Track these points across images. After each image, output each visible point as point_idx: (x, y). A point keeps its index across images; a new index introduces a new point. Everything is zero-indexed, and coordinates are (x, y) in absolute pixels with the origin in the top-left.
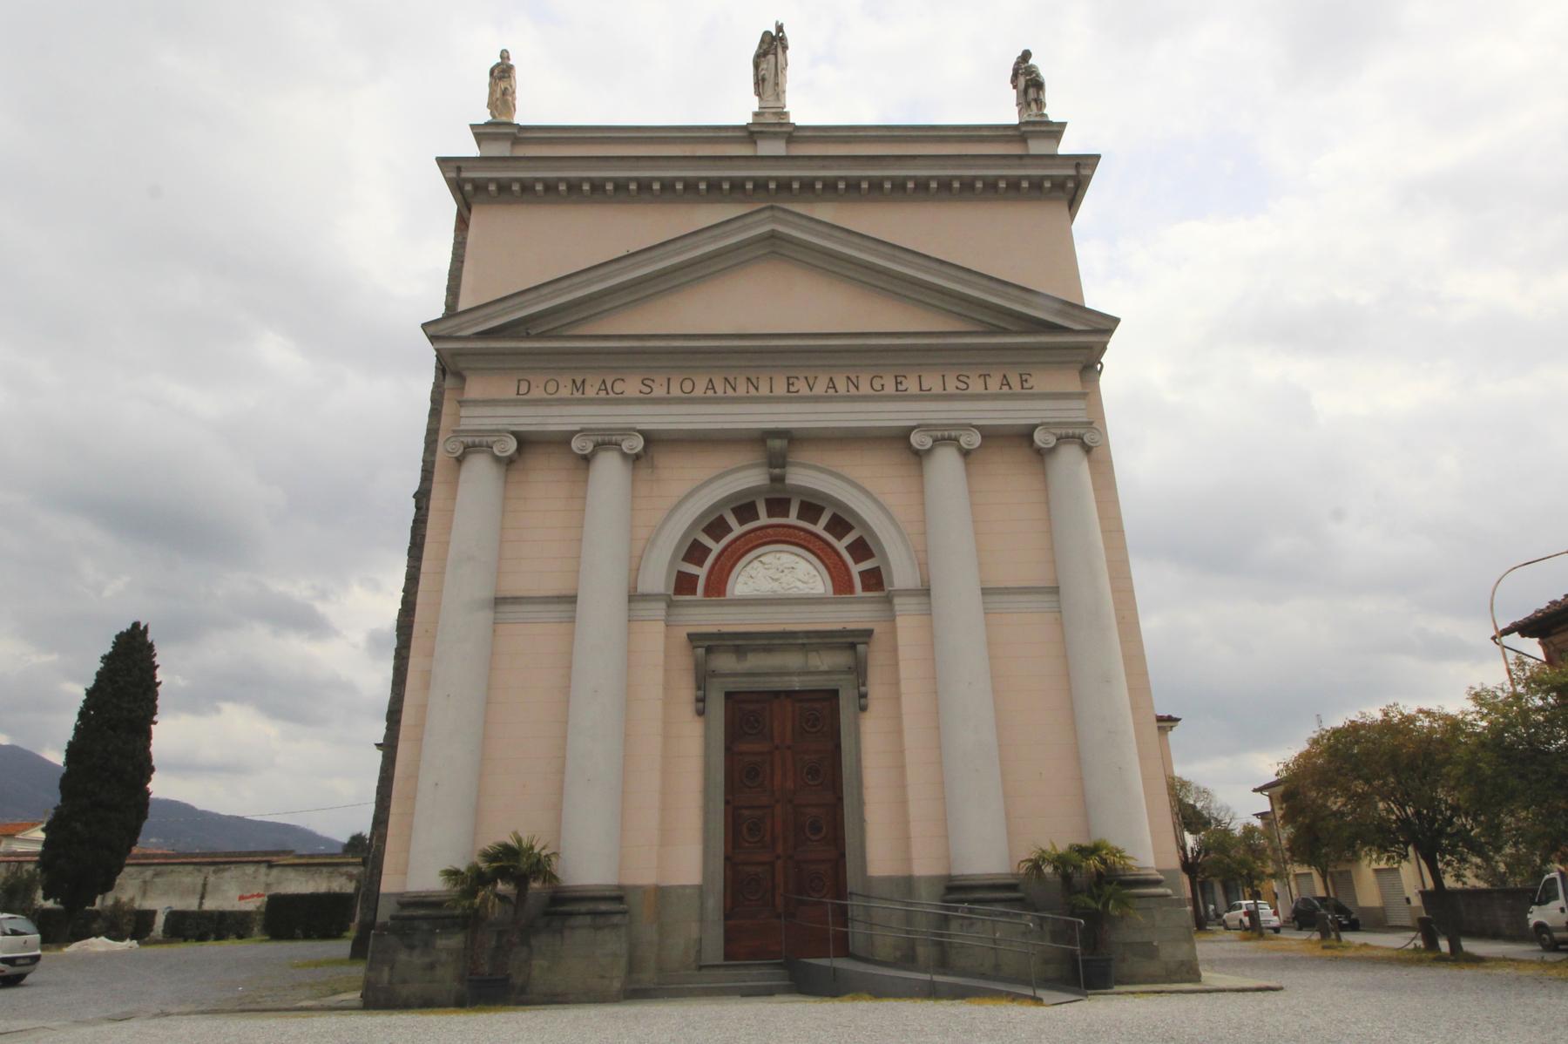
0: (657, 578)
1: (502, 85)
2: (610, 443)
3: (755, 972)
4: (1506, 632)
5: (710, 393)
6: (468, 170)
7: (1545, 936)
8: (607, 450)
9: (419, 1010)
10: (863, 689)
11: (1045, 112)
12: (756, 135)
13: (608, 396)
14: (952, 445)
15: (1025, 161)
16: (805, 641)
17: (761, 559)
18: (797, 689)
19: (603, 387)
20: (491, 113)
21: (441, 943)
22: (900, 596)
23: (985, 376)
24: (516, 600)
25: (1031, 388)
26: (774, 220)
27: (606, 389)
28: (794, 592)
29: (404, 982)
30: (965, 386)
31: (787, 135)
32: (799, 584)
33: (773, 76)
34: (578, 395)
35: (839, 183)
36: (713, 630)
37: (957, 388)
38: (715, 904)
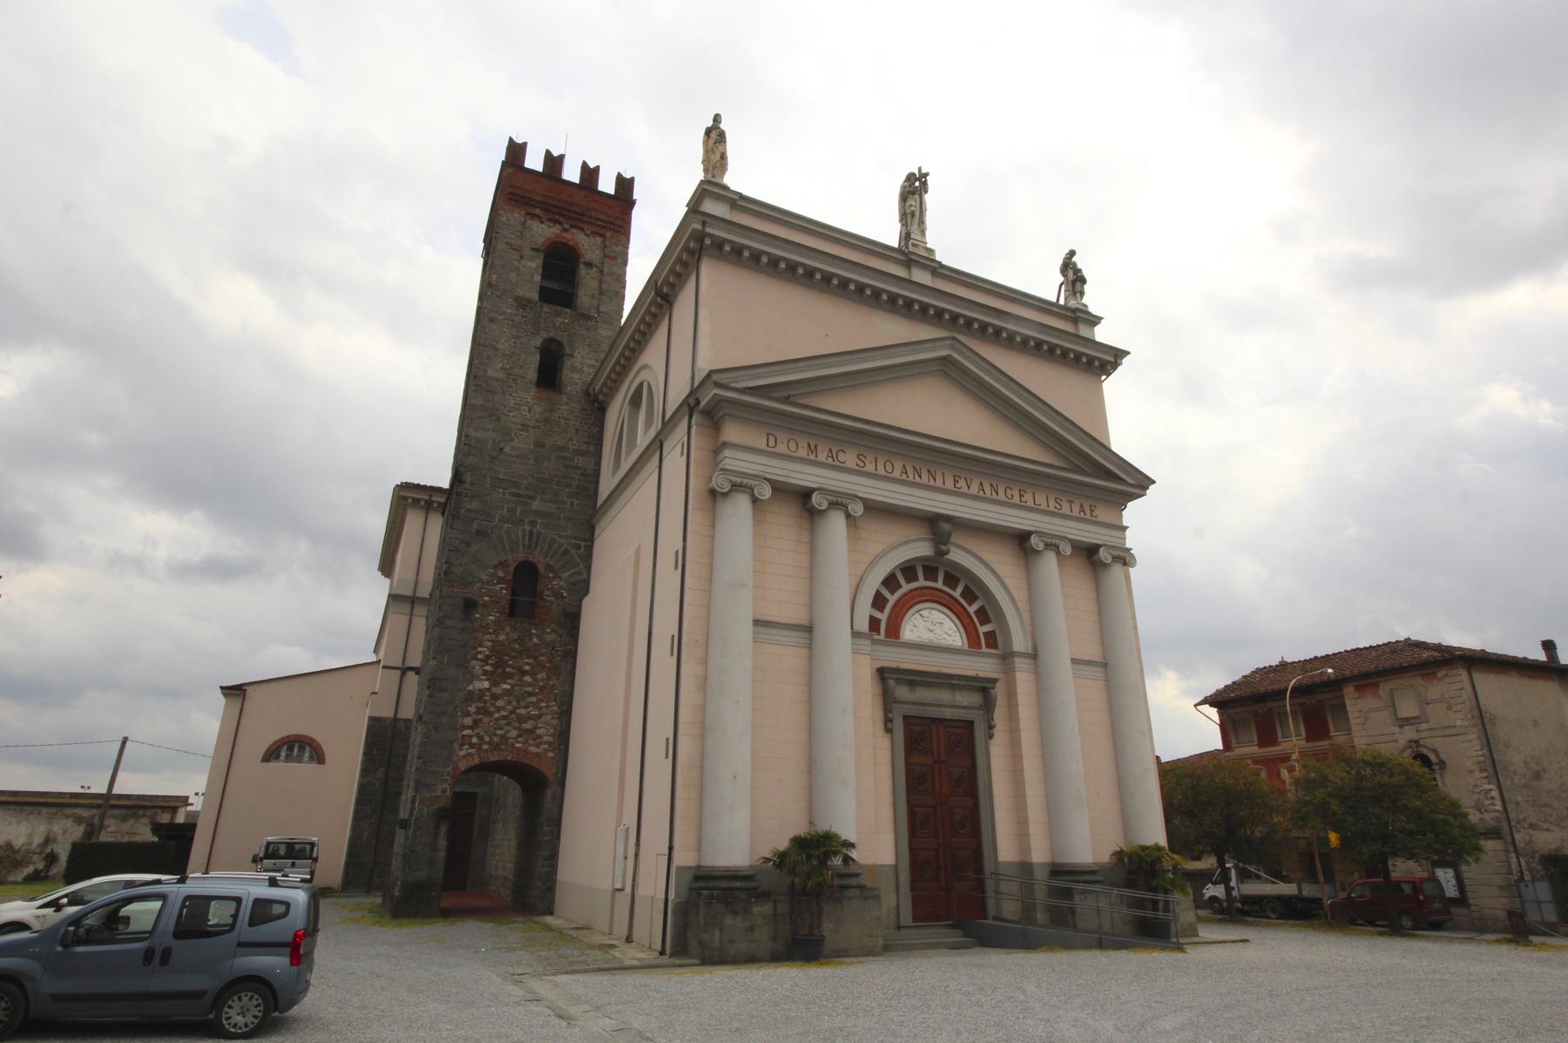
0: (863, 625)
1: (721, 148)
5: (904, 476)
6: (712, 226)
7: (1215, 904)
10: (890, 715)
17: (921, 612)
19: (830, 455)
21: (756, 909)
22: (1018, 656)
27: (832, 457)
29: (732, 942)
32: (946, 637)
34: (812, 457)
36: (935, 669)
37: (857, 465)
38: (905, 877)
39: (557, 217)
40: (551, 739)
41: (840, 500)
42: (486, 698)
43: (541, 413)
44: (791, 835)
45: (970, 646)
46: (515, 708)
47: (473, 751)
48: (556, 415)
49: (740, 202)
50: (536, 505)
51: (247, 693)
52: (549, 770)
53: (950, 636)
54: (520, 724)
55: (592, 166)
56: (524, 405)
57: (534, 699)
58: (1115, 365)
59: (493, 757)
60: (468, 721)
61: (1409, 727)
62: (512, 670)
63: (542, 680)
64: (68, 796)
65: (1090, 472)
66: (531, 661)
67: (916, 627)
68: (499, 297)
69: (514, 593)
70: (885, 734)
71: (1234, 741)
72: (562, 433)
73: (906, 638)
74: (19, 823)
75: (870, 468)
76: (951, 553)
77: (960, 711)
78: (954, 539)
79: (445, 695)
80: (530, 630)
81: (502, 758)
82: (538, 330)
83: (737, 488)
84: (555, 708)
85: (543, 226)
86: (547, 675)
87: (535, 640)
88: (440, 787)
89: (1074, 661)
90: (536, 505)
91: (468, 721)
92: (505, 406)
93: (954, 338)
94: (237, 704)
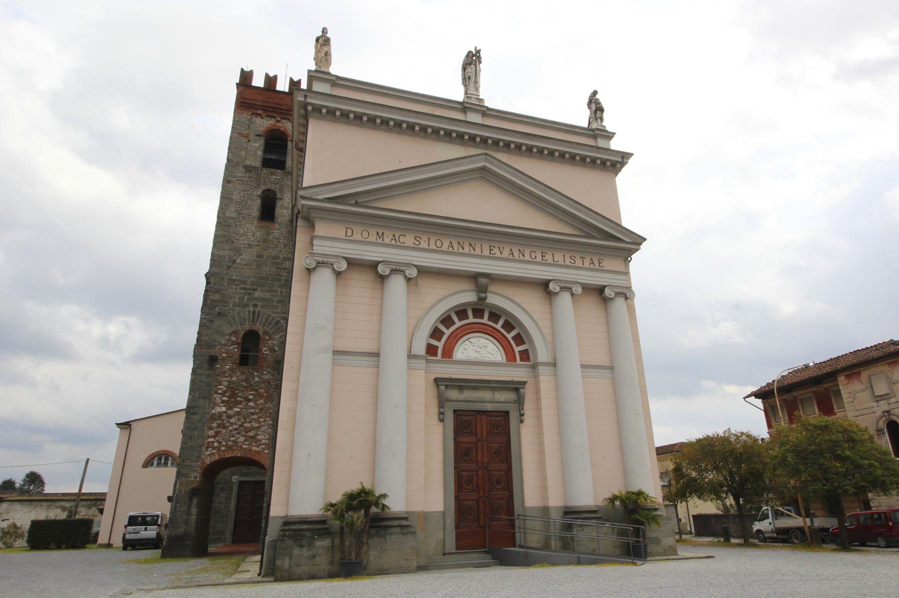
0: (420, 348)
1: (325, 49)
2: (400, 270)
3: (475, 556)
4: (747, 397)
5: (451, 249)
6: (312, 98)
8: (397, 274)
9: (307, 581)
10: (522, 412)
11: (604, 124)
12: (466, 109)
13: (583, 266)
14: (568, 291)
15: (600, 151)
16: (494, 385)
17: (470, 340)
18: (489, 410)
20: (316, 64)
23: (582, 257)
24: (344, 353)
25: (547, 260)
26: (486, 160)
27: (395, 240)
28: (487, 359)
29: (299, 566)
30: (419, 243)
31: (332, 82)
32: (489, 355)
33: (474, 76)
34: (380, 241)
35: (465, 135)
36: (509, 379)
37: (570, 262)
39: (272, 114)
40: (267, 441)
41: (398, 267)
42: (224, 418)
43: (260, 237)
44: (342, 493)
45: (507, 360)
46: (243, 423)
47: (215, 451)
48: (271, 237)
49: (338, 82)
50: (257, 294)
51: (132, 426)
52: (265, 462)
53: (492, 355)
54: (246, 433)
55: (296, 80)
56: (250, 232)
57: (255, 417)
58: (623, 164)
59: (228, 455)
60: (212, 433)
61: (883, 401)
62: (241, 399)
63: (261, 404)
64: (60, 495)
65: (597, 236)
66: (254, 392)
67: (466, 350)
68: (233, 167)
69: (243, 350)
70: (439, 423)
71: (773, 421)
72: (275, 248)
73: (458, 357)
74: (30, 512)
75: (424, 245)
76: (488, 298)
77: (498, 405)
78: (491, 288)
79: (198, 417)
80: (253, 373)
81: (234, 455)
82: (259, 185)
83: (320, 264)
84: (270, 422)
85: (263, 120)
86: (265, 400)
87: (257, 379)
88: (193, 475)
89: (583, 366)
90: (257, 294)
91: (212, 433)
92: (237, 234)
93: (486, 154)
94: (127, 432)
